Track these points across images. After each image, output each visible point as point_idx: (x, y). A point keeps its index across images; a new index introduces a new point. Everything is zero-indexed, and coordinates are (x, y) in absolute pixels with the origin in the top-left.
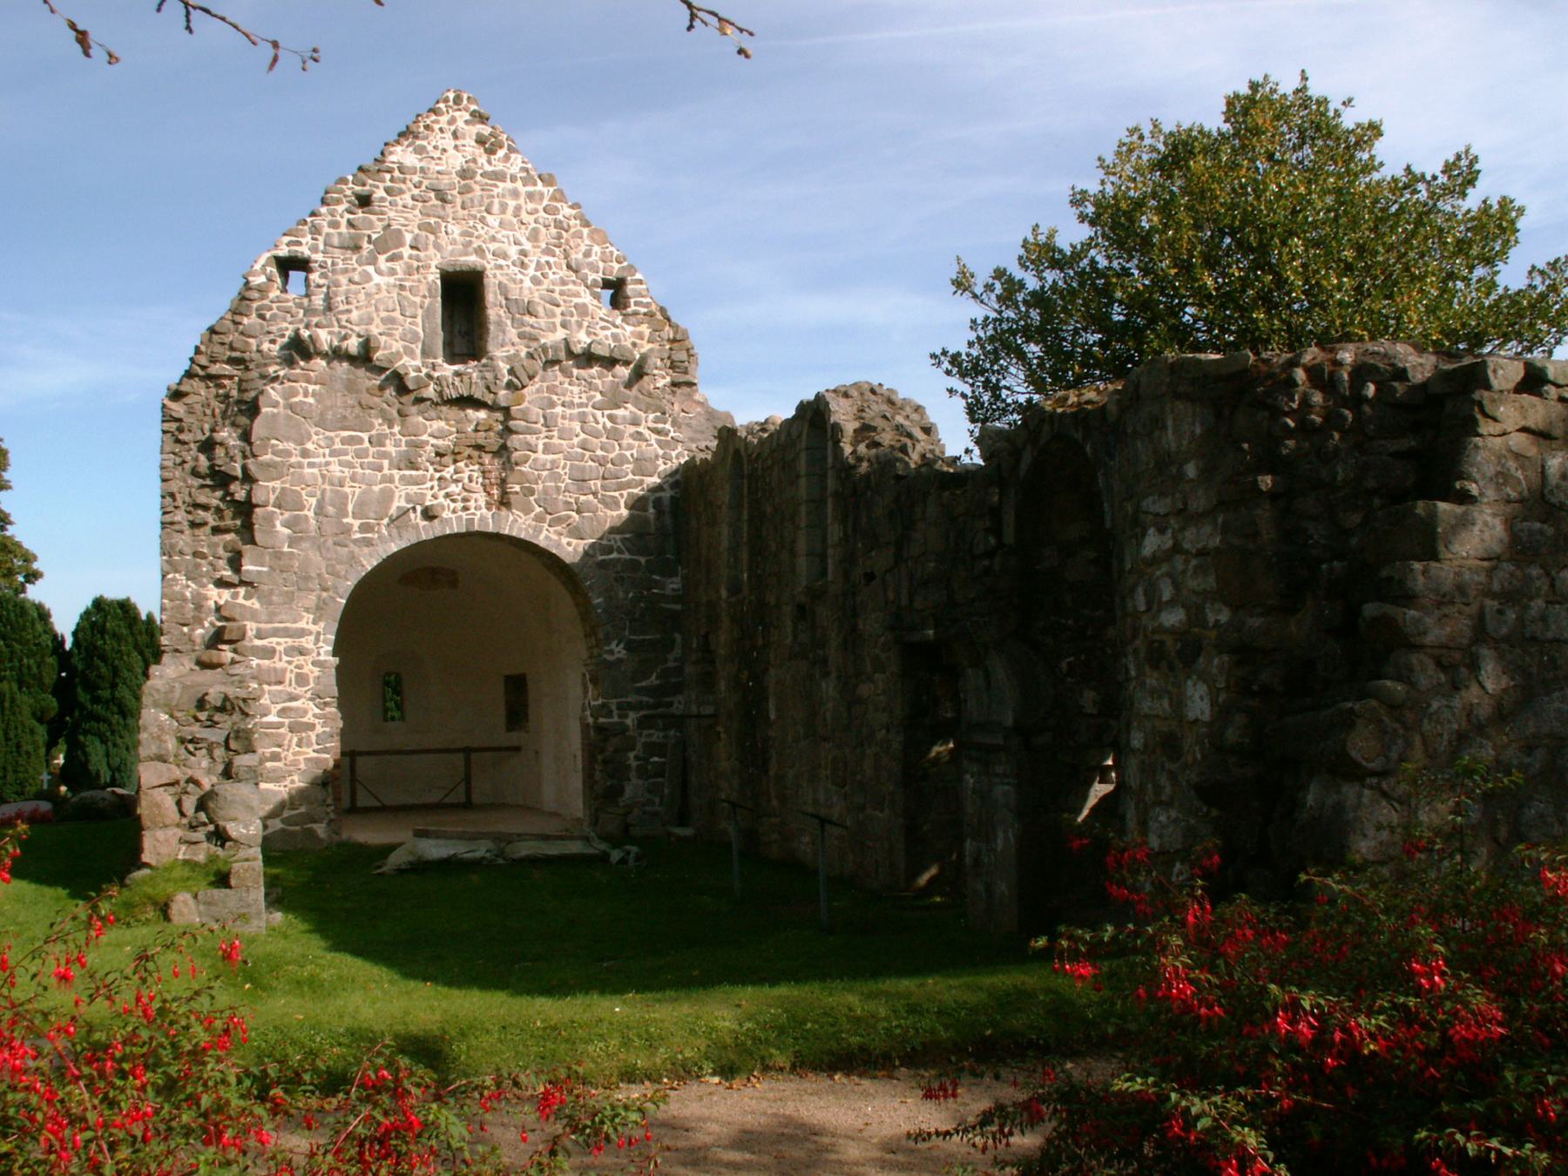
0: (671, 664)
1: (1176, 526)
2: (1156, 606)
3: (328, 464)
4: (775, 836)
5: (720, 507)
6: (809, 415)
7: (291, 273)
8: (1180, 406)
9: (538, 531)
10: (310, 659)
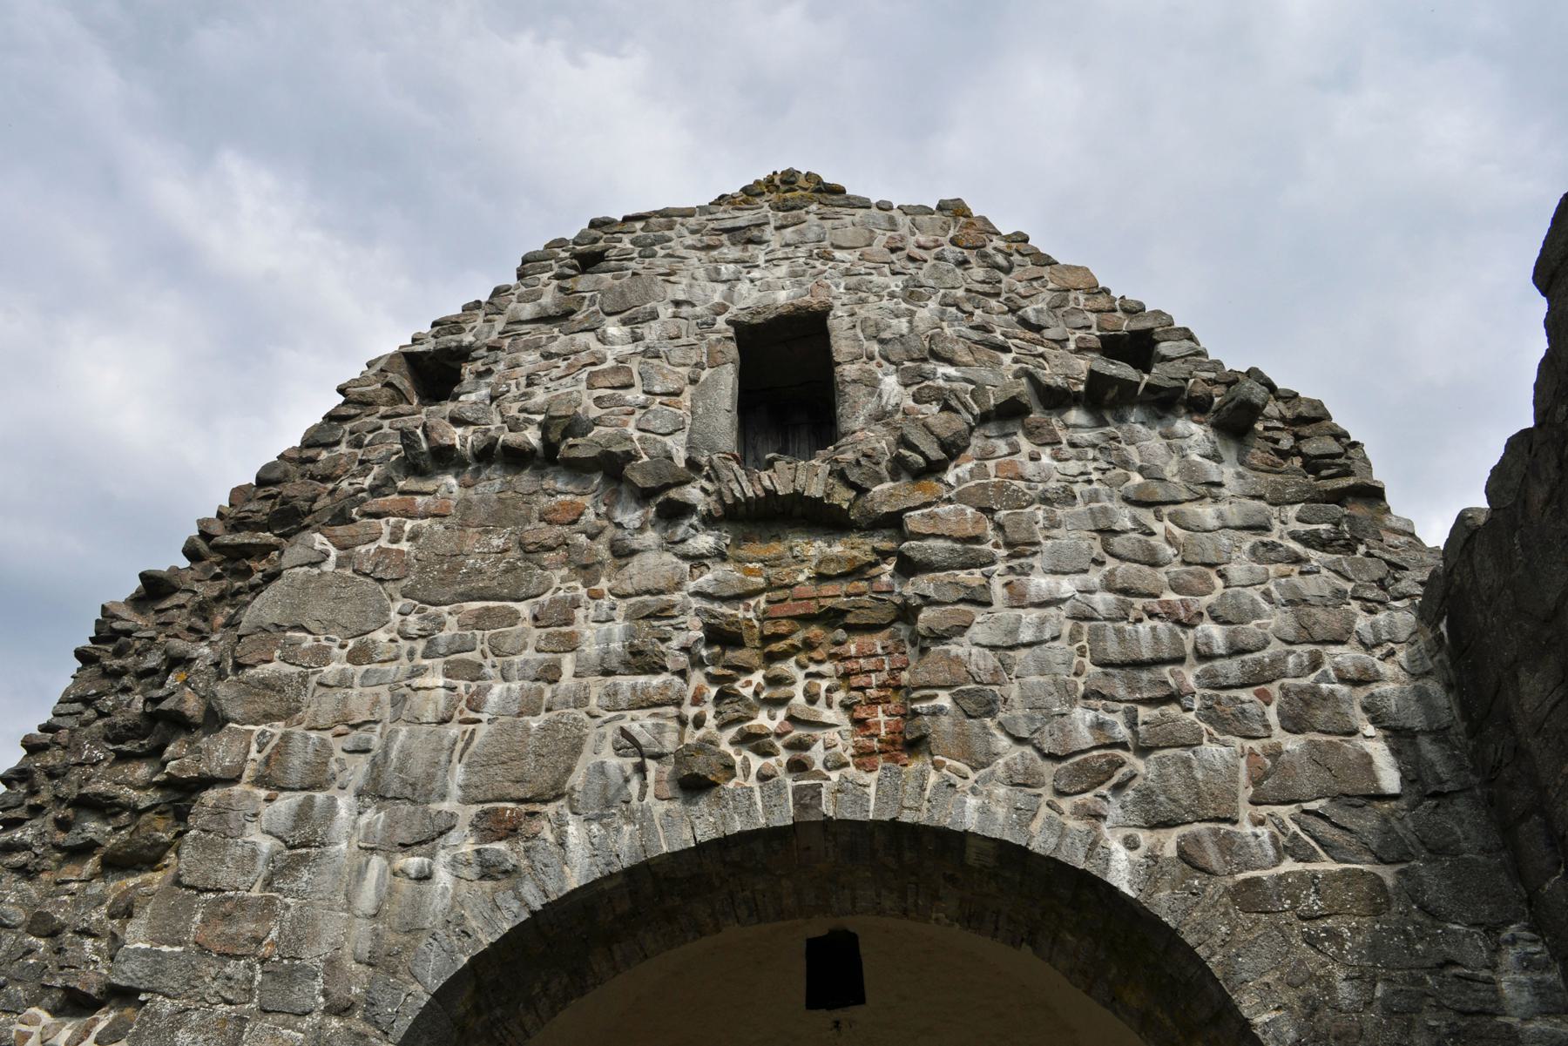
3: (417, 672)
9: (1025, 815)
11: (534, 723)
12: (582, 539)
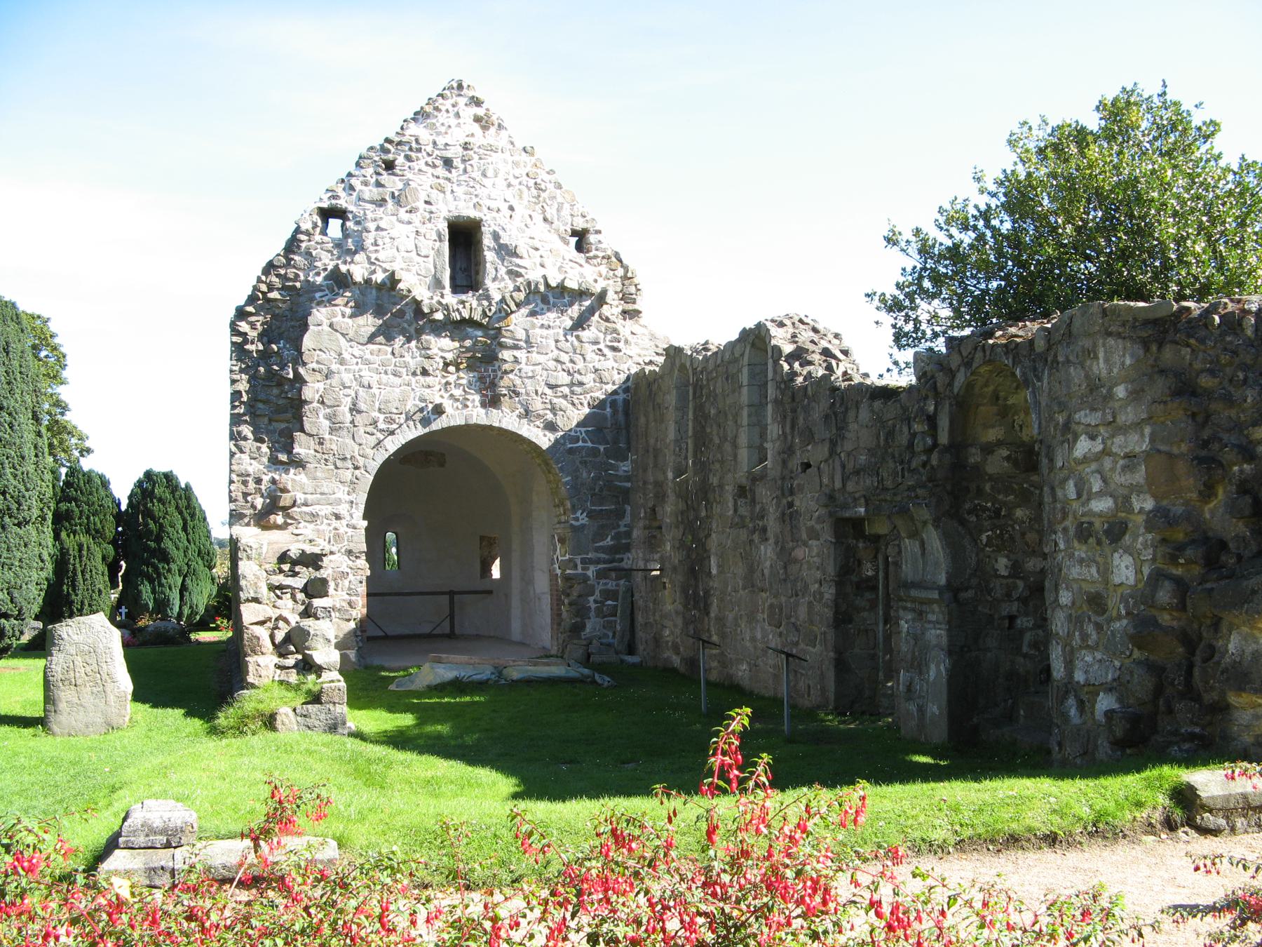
0: (622, 529)
1: (1106, 435)
2: (1083, 492)
3: (360, 370)
4: (715, 664)
5: (667, 408)
6: (752, 337)
7: (330, 220)
8: (1111, 341)
10: (344, 522)
12: (406, 325)
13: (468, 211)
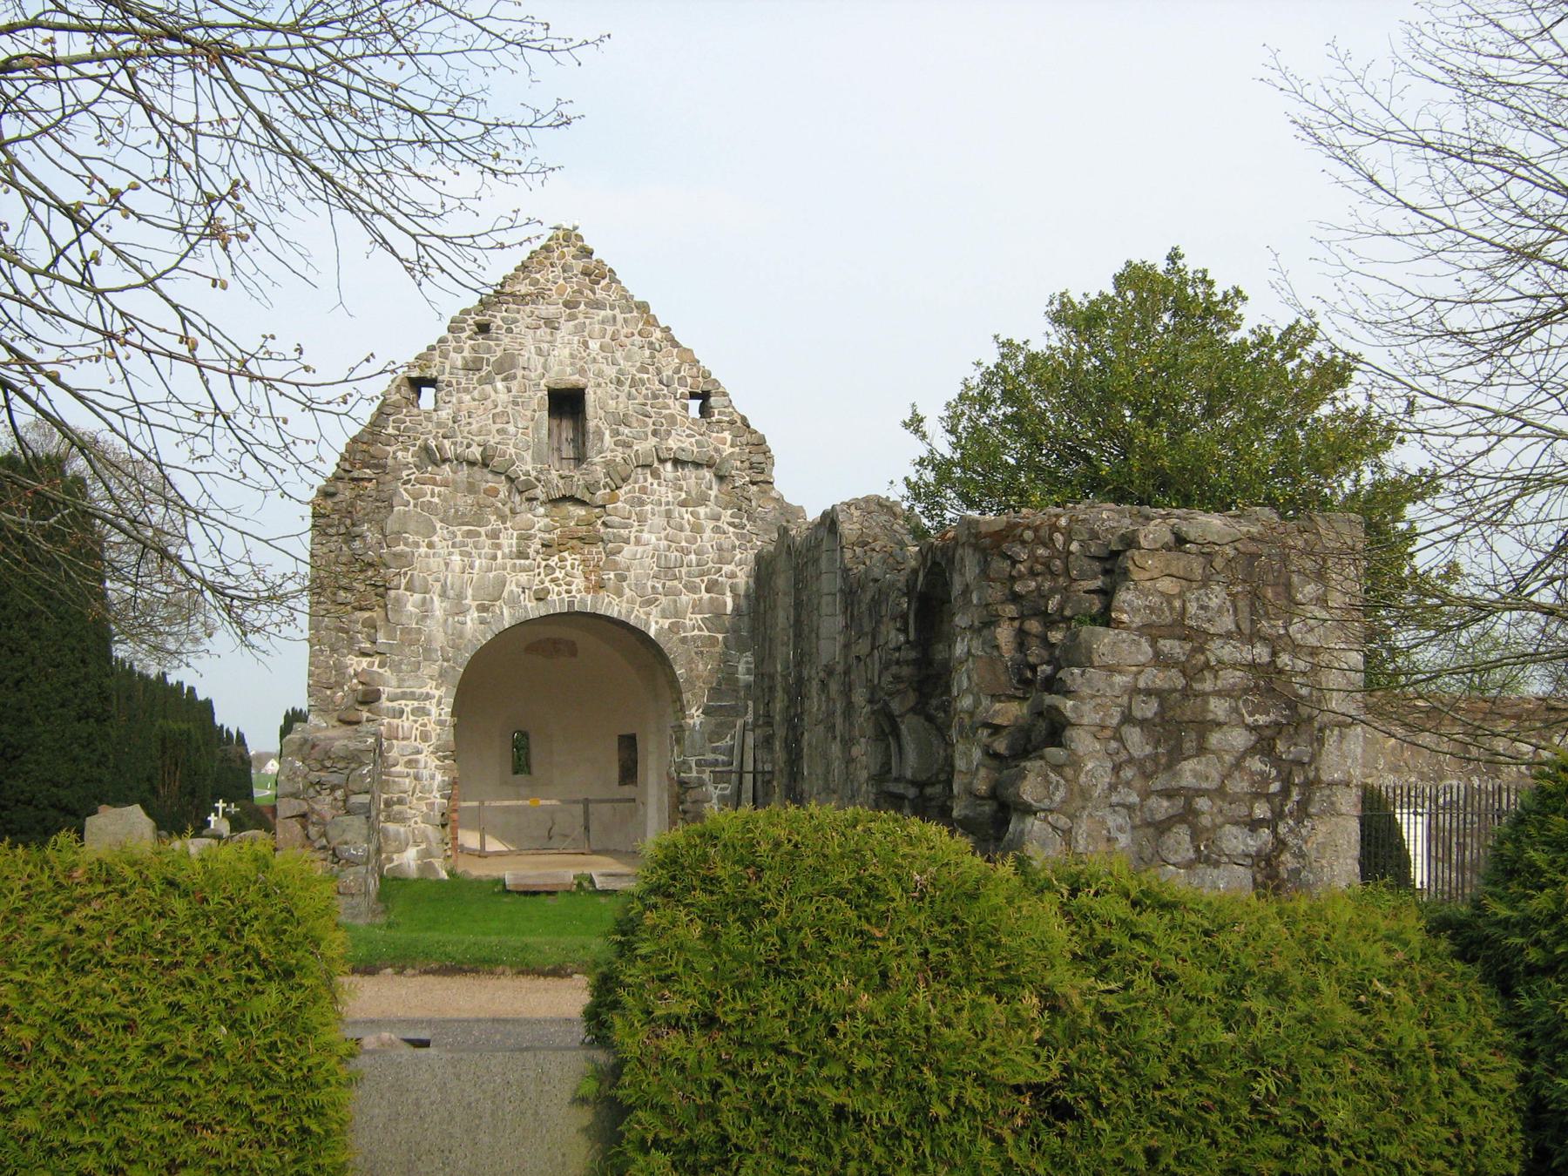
3: (450, 554)
11: (491, 575)
13: (571, 379)
